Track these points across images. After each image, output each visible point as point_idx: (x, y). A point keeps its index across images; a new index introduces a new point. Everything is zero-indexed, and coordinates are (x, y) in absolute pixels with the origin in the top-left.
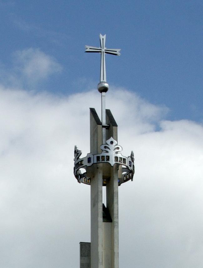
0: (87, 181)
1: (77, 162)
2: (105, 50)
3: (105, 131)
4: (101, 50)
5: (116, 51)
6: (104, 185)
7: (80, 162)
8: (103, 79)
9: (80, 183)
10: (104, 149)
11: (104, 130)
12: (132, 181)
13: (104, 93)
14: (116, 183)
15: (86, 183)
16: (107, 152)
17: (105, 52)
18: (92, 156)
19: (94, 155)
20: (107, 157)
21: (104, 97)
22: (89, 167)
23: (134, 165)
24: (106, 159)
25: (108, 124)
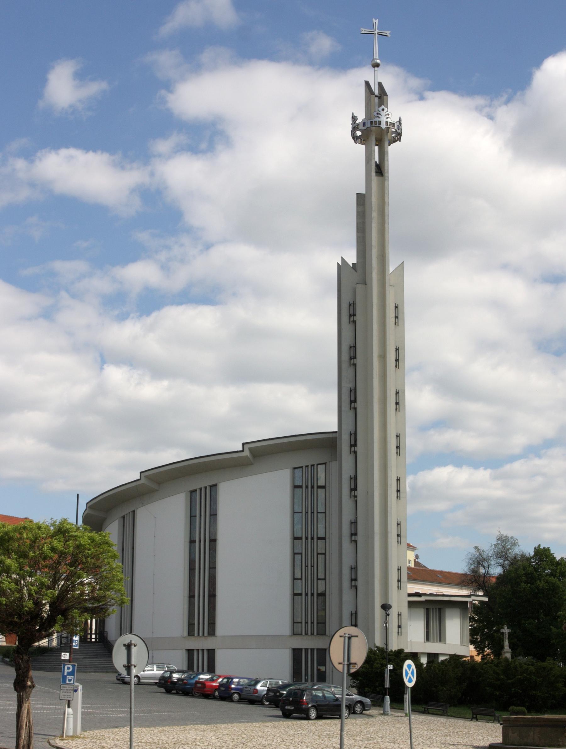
1: (354, 126)
9: (356, 143)
10: (376, 115)
11: (377, 99)
12: (400, 142)
13: (376, 69)
14: (386, 143)
16: (379, 117)
18: (366, 121)
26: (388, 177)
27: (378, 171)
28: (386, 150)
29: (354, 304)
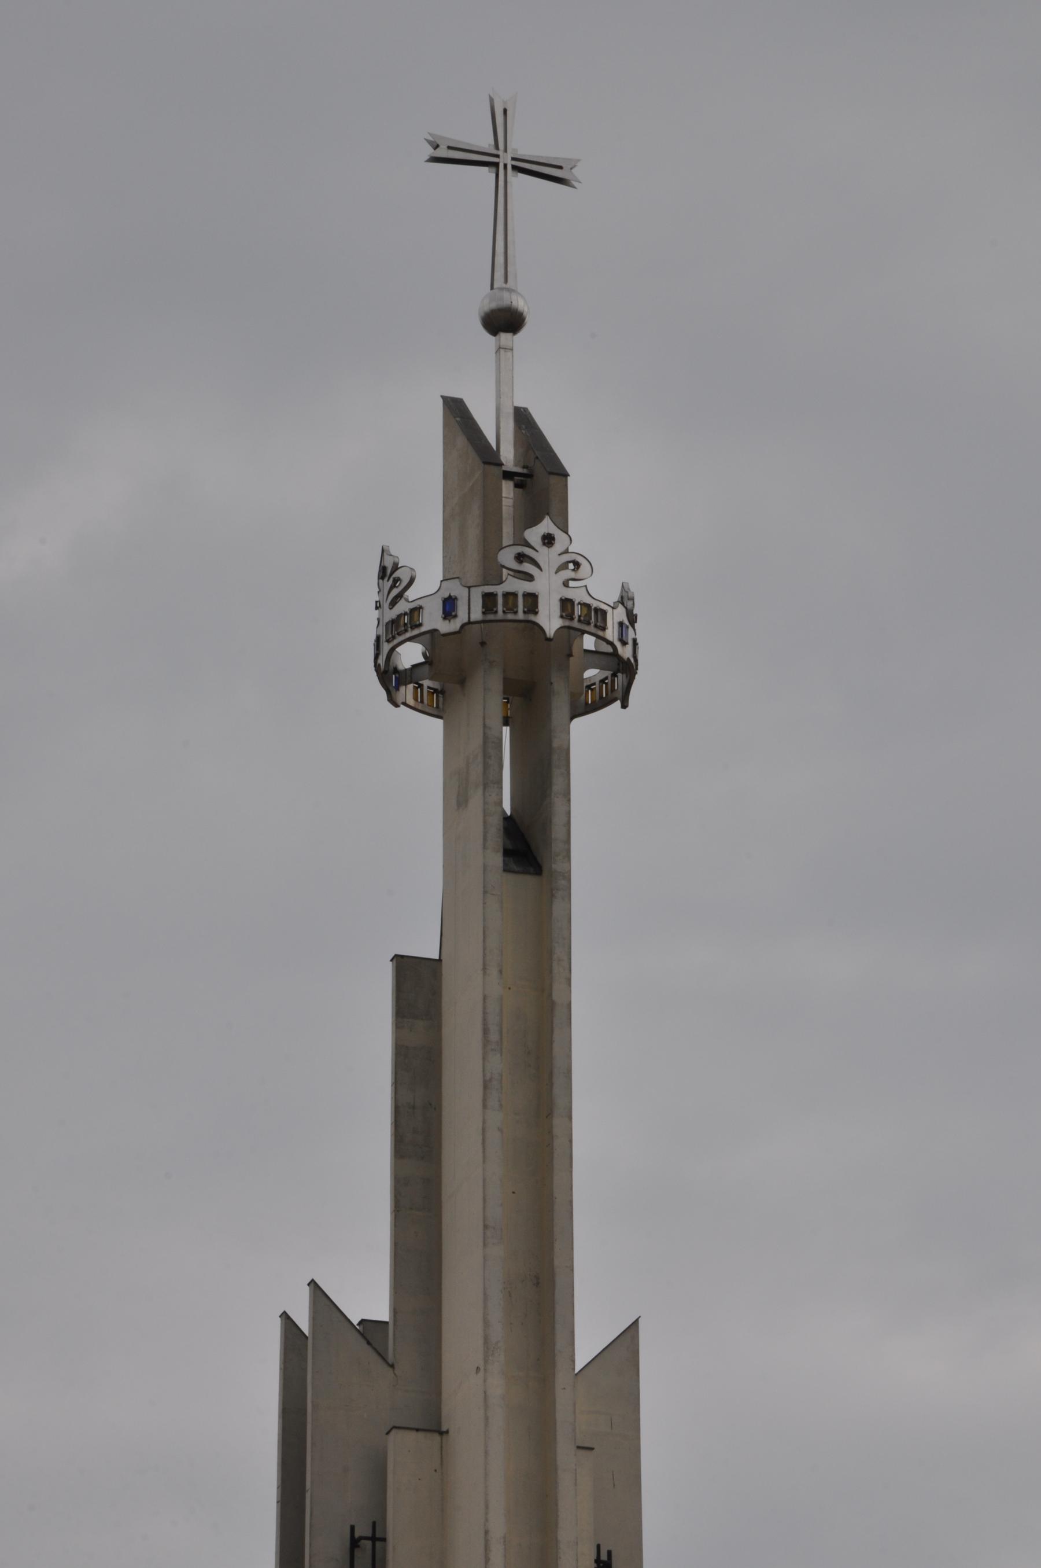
0: (425, 701)
1: (391, 614)
2: (513, 159)
3: (512, 495)
4: (498, 156)
5: (560, 167)
6: (506, 724)
7: (405, 614)
8: (503, 280)
9: (396, 705)
10: (515, 566)
11: (508, 489)
12: (624, 706)
13: (505, 337)
14: (560, 705)
15: (420, 707)
16: (530, 578)
17: (514, 168)
18: (456, 589)
19: (472, 589)
20: (530, 600)
21: (509, 354)
22: (445, 635)
23: (638, 641)
24: (524, 607)
25: (524, 467)
26: (568, 879)
27: (510, 847)
28: (556, 743)
29: (374, 1539)
